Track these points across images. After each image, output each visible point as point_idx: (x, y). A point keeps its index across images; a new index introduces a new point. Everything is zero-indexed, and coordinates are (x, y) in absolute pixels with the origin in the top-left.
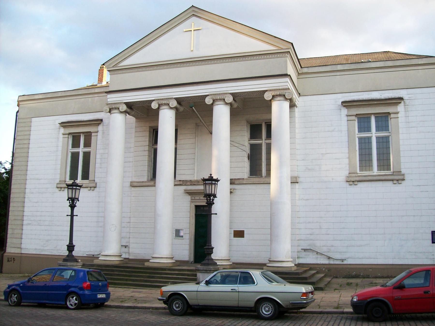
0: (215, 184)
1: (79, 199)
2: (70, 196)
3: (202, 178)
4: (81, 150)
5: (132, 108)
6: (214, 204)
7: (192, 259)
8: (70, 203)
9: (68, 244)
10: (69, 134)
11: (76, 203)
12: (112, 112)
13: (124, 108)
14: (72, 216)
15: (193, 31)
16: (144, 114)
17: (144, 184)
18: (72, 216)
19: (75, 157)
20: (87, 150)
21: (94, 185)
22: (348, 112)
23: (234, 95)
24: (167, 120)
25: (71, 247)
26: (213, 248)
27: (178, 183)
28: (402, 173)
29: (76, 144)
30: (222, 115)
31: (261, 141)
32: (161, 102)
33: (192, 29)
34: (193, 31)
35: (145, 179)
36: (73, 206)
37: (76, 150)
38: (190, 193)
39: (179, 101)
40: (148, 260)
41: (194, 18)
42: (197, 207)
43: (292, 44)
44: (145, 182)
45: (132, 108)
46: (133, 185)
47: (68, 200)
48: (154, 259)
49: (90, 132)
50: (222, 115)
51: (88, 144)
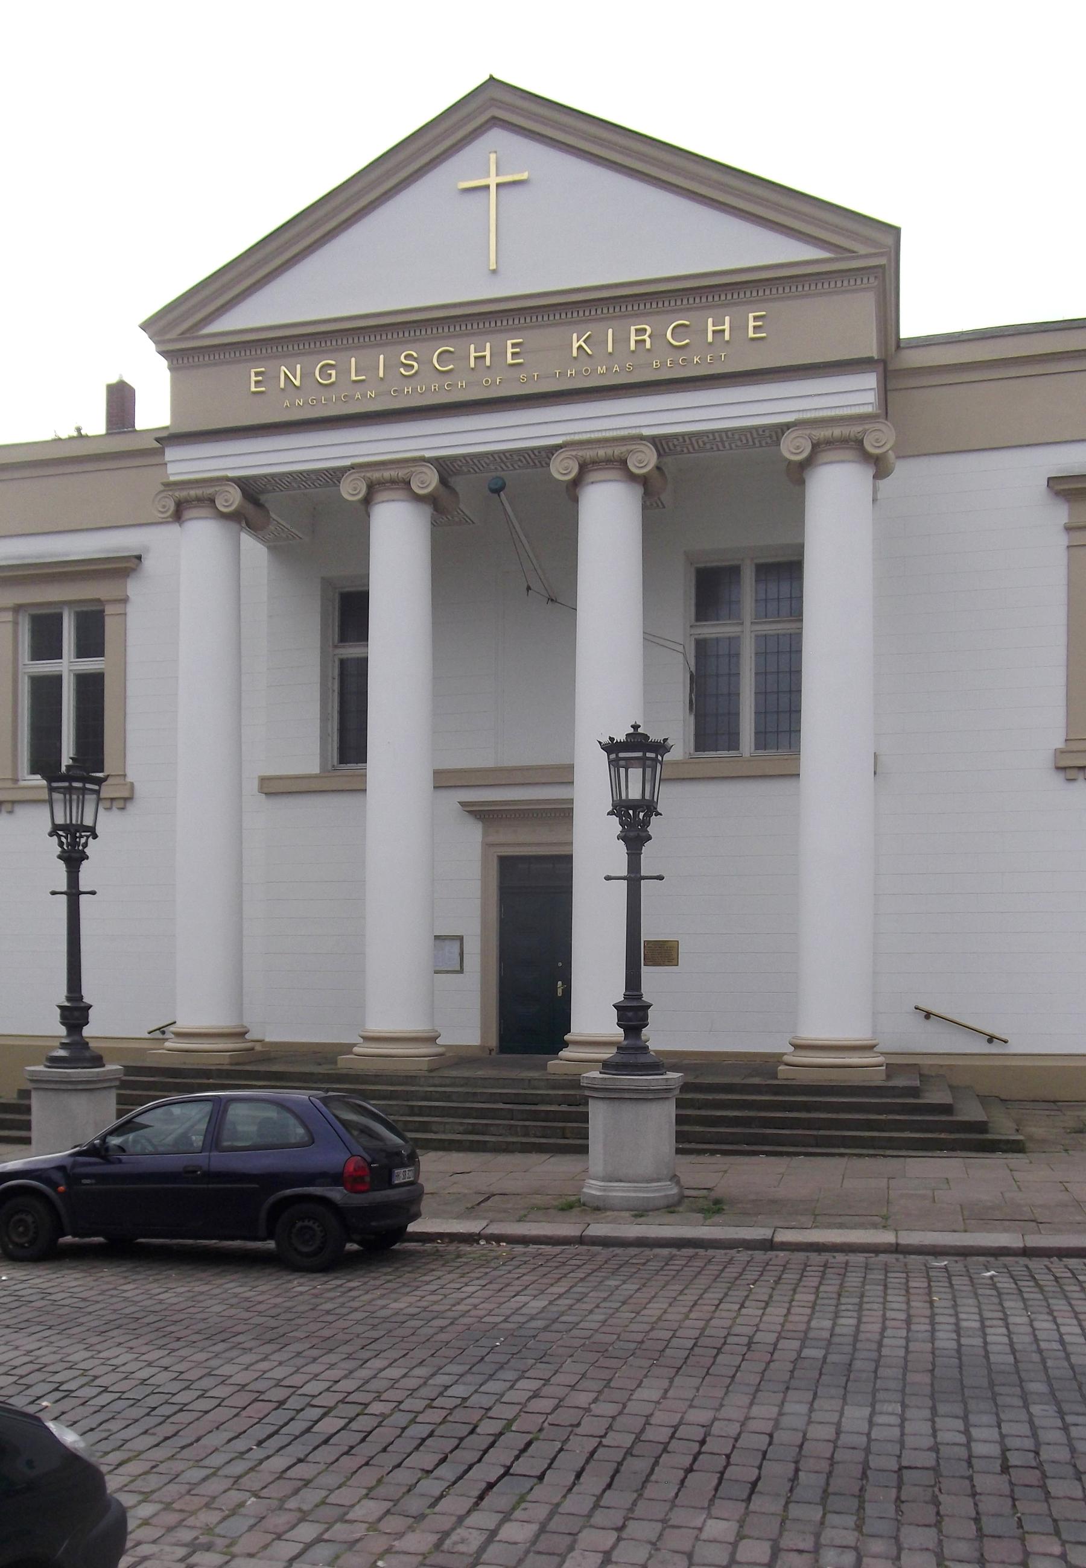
0: (655, 760)
1: (97, 832)
2: (60, 820)
3: (605, 740)
4: (68, 666)
5: (254, 505)
6: (649, 838)
7: (493, 1042)
8: (61, 844)
9: (620, 998)
10: (17, 609)
11: (86, 845)
12: (187, 514)
13: (233, 498)
14: (73, 894)
15: (493, 189)
16: (304, 529)
17: (315, 785)
18: (73, 894)
19: (46, 691)
20: (90, 665)
21: (126, 794)
22: (1070, 515)
23: (662, 444)
24: (397, 549)
25: (75, 1014)
26: (90, 1007)
27: (444, 780)
28: (129, 779)
29: (46, 644)
30: (608, 524)
31: (738, 629)
32: (376, 475)
33: (493, 181)
34: (493, 189)
35: (313, 767)
36: (73, 859)
37: (46, 667)
38: (485, 815)
39: (447, 469)
40: (348, 1048)
41: (497, 137)
42: (506, 863)
43: (496, 109)
44: (315, 777)
45: (254, 505)
46: (274, 788)
47: (51, 835)
48: (803, 1053)
49: (99, 601)
50: (608, 524)
51: (92, 641)
